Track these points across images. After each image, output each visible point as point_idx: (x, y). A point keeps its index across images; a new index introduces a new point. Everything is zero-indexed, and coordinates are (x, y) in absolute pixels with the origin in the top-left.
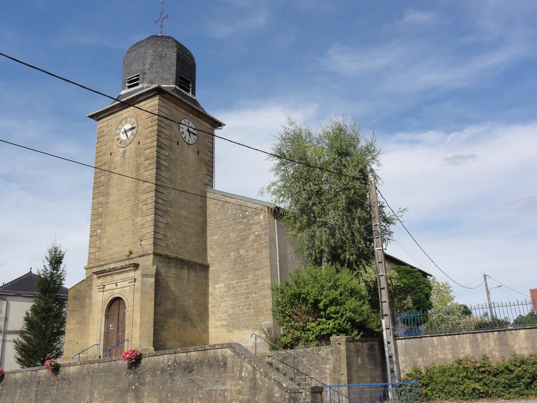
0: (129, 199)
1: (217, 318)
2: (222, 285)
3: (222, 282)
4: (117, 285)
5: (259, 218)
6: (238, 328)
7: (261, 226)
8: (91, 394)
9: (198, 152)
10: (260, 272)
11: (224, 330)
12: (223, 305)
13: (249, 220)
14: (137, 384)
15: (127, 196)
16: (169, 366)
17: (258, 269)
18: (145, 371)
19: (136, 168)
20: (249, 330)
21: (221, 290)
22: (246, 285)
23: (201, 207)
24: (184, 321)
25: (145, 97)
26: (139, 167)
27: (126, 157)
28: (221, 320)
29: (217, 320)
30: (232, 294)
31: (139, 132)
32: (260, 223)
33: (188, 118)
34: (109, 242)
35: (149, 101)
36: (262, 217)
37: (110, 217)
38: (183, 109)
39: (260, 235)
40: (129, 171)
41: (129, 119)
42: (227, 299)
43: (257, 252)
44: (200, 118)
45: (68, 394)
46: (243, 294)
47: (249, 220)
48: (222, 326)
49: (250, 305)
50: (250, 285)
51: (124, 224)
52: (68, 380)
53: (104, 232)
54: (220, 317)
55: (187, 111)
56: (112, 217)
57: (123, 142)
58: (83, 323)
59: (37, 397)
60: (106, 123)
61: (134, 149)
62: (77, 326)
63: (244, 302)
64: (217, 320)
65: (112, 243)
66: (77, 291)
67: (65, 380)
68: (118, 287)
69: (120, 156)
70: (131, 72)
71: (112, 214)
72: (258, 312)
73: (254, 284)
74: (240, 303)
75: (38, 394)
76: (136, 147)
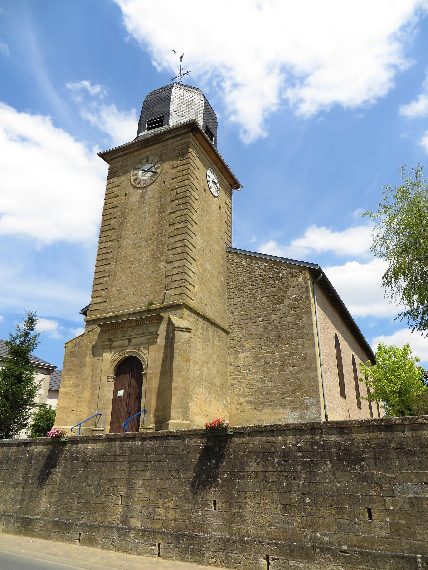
0: (149, 242)
1: (240, 393)
2: (248, 354)
3: (247, 351)
4: (130, 342)
5: (297, 280)
6: (270, 406)
7: (299, 289)
8: (130, 486)
9: (220, 207)
10: (300, 341)
11: (250, 408)
12: (248, 378)
13: (283, 282)
14: (226, 476)
15: (146, 240)
16: (299, 449)
17: (296, 338)
18: (244, 456)
19: (160, 209)
20: (287, 408)
21: (245, 360)
22: (281, 356)
23: (222, 265)
24: (209, 392)
25: (174, 135)
26: (165, 208)
27: (146, 197)
28: (245, 396)
29: (240, 395)
30: (261, 366)
31: (164, 171)
32: (298, 285)
33: (213, 168)
34: (119, 291)
35: (178, 138)
36: (300, 279)
37: (122, 263)
38: (210, 156)
39: (299, 300)
40: (149, 212)
41: (150, 159)
42: (254, 371)
43: (296, 319)
44: (222, 172)
45: (84, 482)
46: (277, 365)
47: (283, 282)
48: (248, 402)
49: (286, 379)
50: (286, 356)
51: (141, 270)
52: (83, 460)
53: (114, 280)
54: (244, 392)
55: (212, 160)
56: (126, 262)
57: (142, 182)
58: (81, 386)
59: (27, 481)
60: (121, 163)
61: (157, 189)
62: (73, 389)
63: (278, 375)
64: (240, 395)
65: (124, 292)
66: (75, 346)
67: (78, 460)
68: (131, 343)
69: (138, 197)
70: (153, 113)
71: (126, 260)
72: (299, 387)
73: (292, 354)
74: (272, 376)
75: (28, 477)
76: (160, 186)
